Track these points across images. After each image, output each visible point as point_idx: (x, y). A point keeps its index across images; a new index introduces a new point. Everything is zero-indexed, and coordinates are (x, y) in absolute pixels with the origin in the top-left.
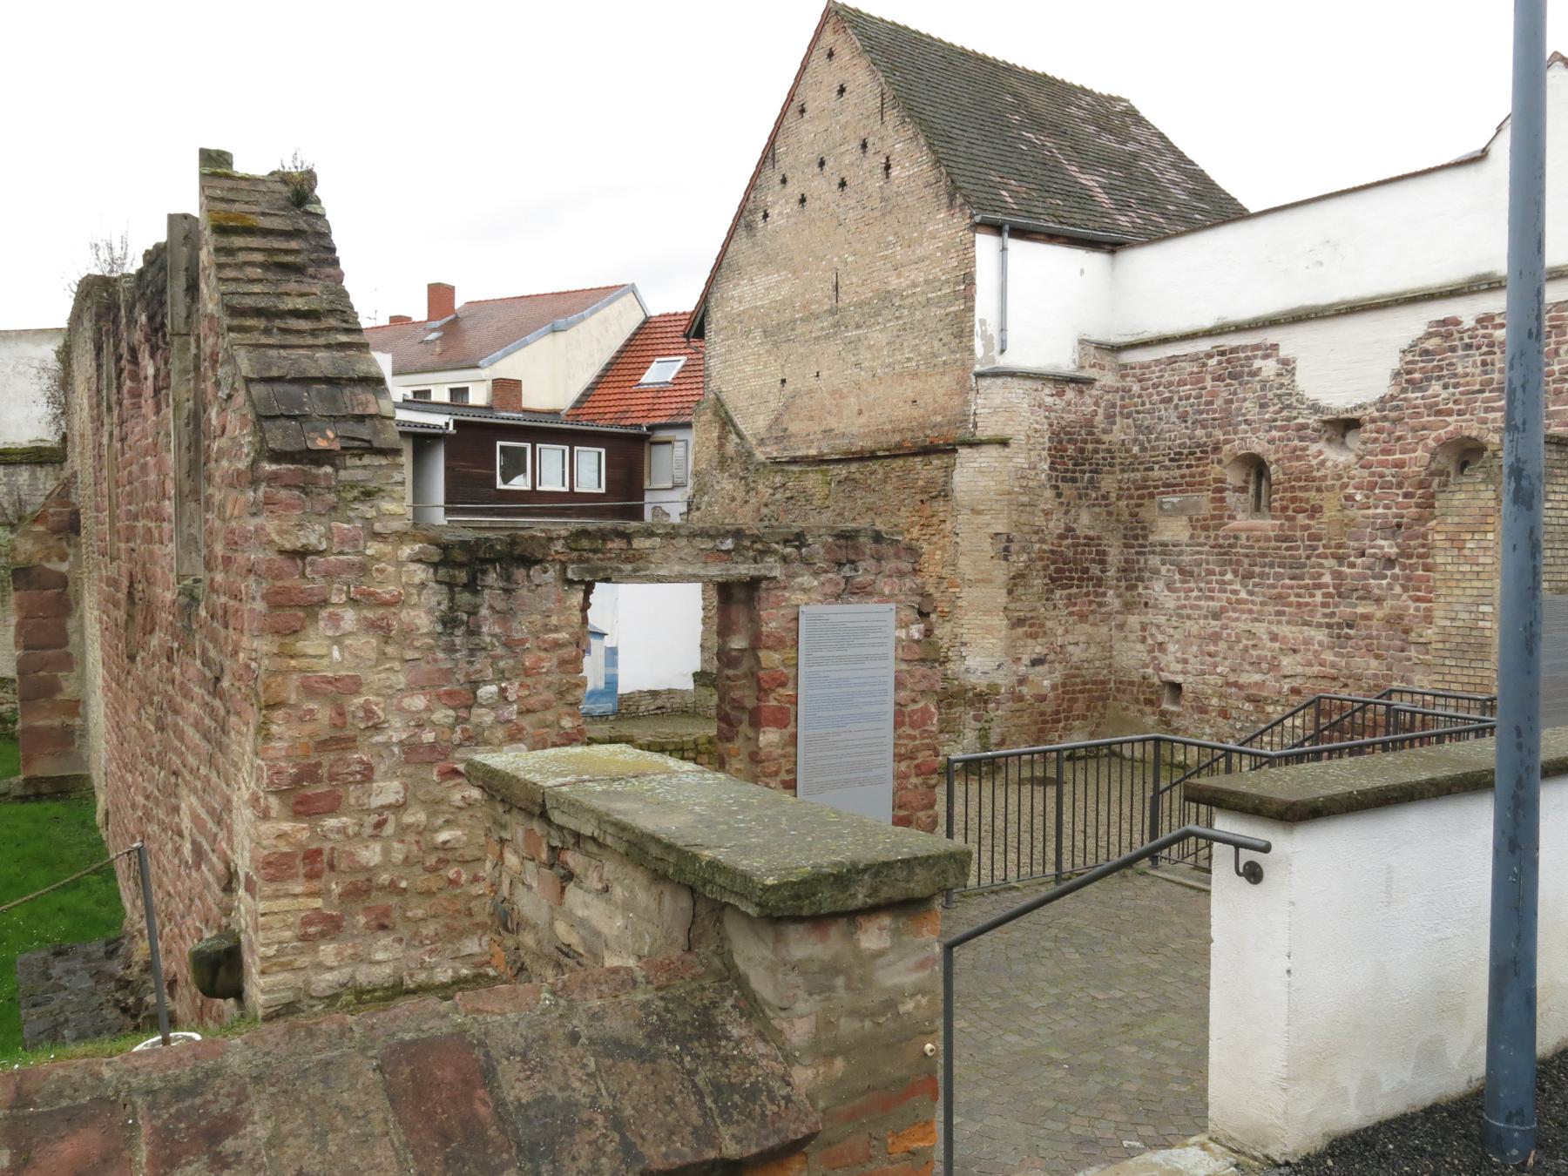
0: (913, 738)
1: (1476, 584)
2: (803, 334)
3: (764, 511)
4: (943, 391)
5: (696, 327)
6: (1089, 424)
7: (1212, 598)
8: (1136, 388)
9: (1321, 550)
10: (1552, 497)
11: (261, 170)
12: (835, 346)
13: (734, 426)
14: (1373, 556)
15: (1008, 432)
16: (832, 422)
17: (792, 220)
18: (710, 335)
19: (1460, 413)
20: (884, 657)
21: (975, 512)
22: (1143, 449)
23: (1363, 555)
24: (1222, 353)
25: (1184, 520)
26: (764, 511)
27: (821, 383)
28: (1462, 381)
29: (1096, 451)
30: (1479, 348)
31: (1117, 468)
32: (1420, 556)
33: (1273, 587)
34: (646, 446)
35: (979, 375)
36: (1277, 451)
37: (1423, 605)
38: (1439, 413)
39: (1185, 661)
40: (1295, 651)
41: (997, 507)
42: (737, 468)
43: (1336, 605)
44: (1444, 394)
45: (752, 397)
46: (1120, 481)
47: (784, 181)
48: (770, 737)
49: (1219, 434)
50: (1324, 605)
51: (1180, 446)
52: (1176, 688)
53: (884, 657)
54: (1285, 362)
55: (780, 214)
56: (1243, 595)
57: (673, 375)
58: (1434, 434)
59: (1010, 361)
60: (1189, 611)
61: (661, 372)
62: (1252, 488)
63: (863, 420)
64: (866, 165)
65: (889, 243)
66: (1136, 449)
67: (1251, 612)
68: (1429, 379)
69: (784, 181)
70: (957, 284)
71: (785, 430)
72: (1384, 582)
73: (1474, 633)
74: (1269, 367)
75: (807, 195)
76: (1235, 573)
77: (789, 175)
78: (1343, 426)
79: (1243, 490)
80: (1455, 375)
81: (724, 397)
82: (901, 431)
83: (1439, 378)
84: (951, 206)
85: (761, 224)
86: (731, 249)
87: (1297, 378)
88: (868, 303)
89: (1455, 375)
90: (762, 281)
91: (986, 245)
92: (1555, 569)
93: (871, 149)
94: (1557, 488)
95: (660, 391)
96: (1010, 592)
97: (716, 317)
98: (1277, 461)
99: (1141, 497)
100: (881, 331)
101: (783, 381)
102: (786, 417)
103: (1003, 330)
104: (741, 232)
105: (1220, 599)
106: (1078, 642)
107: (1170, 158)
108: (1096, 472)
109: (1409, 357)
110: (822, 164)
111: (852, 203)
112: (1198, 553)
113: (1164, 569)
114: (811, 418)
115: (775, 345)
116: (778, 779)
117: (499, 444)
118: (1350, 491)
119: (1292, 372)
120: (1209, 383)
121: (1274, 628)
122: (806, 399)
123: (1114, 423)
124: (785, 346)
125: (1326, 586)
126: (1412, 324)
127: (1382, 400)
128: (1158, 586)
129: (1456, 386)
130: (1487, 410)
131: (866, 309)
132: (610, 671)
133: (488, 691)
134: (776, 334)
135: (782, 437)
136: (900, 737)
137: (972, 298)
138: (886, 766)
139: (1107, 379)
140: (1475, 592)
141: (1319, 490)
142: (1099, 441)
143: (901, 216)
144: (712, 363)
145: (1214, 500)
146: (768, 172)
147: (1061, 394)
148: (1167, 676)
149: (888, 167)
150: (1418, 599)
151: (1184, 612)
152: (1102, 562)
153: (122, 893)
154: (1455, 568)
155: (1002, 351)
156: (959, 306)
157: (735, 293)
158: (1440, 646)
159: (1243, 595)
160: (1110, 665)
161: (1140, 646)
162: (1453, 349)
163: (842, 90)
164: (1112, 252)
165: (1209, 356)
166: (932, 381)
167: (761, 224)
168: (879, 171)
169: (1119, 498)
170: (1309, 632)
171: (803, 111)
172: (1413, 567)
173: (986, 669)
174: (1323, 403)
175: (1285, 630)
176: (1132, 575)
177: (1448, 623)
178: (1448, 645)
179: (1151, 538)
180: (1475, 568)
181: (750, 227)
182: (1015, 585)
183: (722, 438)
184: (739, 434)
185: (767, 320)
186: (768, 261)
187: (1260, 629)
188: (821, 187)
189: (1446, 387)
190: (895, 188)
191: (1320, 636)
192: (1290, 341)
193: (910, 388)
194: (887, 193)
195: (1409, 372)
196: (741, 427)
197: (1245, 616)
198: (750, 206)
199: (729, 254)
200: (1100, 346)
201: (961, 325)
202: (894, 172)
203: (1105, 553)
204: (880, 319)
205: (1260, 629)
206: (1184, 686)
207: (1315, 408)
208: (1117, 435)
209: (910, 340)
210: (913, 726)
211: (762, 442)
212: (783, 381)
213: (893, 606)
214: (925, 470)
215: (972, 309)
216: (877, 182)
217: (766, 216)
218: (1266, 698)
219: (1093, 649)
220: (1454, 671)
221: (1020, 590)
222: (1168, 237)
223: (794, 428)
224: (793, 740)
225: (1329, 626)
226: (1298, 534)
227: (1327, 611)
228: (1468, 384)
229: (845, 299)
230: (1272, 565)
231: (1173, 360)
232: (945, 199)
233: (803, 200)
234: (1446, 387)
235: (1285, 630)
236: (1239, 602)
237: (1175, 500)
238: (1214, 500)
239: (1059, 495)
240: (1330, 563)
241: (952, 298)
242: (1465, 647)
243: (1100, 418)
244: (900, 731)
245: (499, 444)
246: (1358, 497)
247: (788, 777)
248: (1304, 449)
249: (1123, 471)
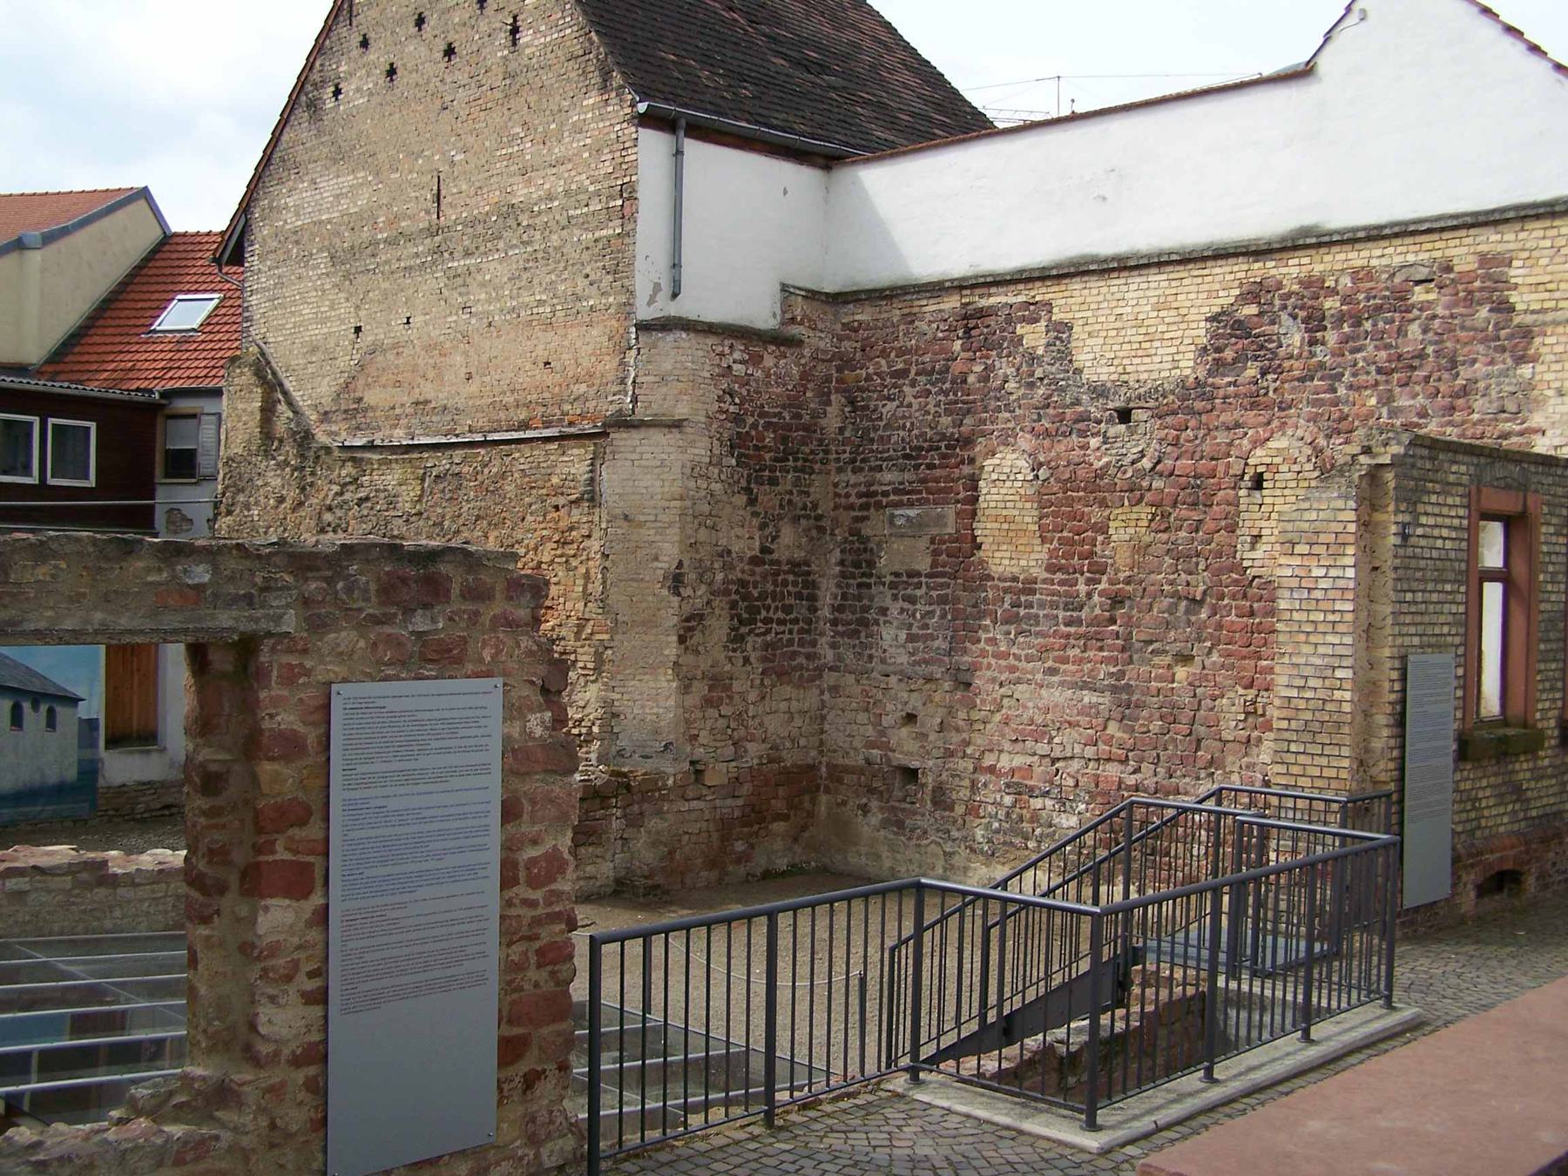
0: (533, 904)
1: (1330, 639)
2: (387, 262)
3: (328, 517)
4: (589, 349)
5: (232, 248)
10: (1423, 520)
12: (435, 280)
13: (285, 393)
16: (428, 391)
17: (376, 100)
18: (252, 261)
20: (484, 769)
26: (328, 517)
27: (412, 333)
31: (833, 465)
34: (160, 420)
42: (290, 450)
45: (314, 350)
46: (836, 485)
47: (365, 44)
48: (278, 918)
52: (911, 774)
53: (484, 769)
55: (358, 90)
57: (199, 321)
59: (686, 307)
61: (184, 314)
63: (474, 387)
64: (483, 26)
65: (514, 137)
69: (365, 44)
70: (611, 197)
71: (360, 399)
73: (1329, 707)
75: (398, 64)
77: (371, 35)
81: (269, 350)
82: (527, 405)
84: (604, 88)
85: (330, 104)
86: (285, 137)
88: (483, 220)
90: (329, 186)
92: (1426, 619)
94: (1429, 509)
95: (184, 339)
96: (682, 640)
97: (262, 232)
100: (501, 260)
101: (358, 330)
102: (361, 382)
104: (302, 115)
106: (778, 719)
107: (901, 55)
108: (802, 470)
110: (420, 22)
111: (462, 78)
114: (398, 384)
115: (347, 276)
116: (292, 989)
117: (93, 426)
122: (390, 356)
123: (829, 403)
124: (361, 279)
126: (1219, 288)
131: (480, 229)
132: (87, 754)
134: (350, 258)
135: (355, 412)
136: (509, 903)
137: (633, 218)
138: (489, 954)
139: (816, 341)
143: (532, 99)
144: (254, 300)
146: (342, 30)
147: (756, 360)
148: (899, 758)
149: (515, 30)
152: (813, 598)
155: (675, 295)
156: (615, 228)
157: (291, 202)
158: (1284, 724)
160: (822, 743)
164: (827, 168)
166: (573, 333)
167: (330, 104)
168: (503, 38)
176: (857, 623)
177: (1294, 693)
178: (1294, 725)
180: (1331, 617)
181: (314, 106)
182: (691, 629)
183: (268, 411)
184: (290, 404)
185: (337, 241)
186: (339, 157)
188: (418, 54)
190: (525, 61)
192: (1069, 301)
193: (544, 343)
194: (513, 66)
195: (1219, 350)
196: (296, 395)
198: (315, 76)
199: (283, 145)
200: (812, 295)
202: (525, 37)
203: (814, 585)
204: (501, 245)
209: (543, 275)
210: (533, 883)
211: (325, 417)
212: (358, 330)
213: (499, 681)
216: (499, 48)
217: (337, 92)
218: (1032, 789)
219: (798, 722)
220: (1301, 759)
221: (697, 637)
222: (905, 153)
223: (372, 397)
224: (322, 917)
229: (450, 215)
232: (596, 79)
233: (392, 72)
237: (912, 513)
239: (752, 502)
241: (603, 217)
242: (1316, 727)
244: (510, 893)
245: (93, 426)
247: (311, 985)
249: (840, 470)
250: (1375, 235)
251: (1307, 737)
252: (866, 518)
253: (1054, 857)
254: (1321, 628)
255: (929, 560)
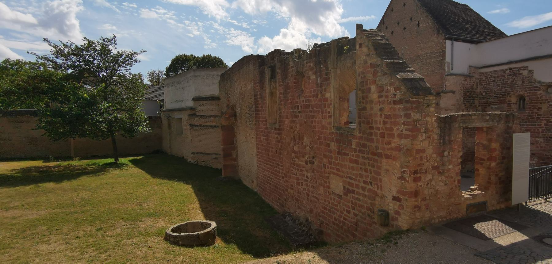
6: (472, 88)
8: (484, 79)
11: (368, 29)
15: (454, 90)
22: (486, 94)
24: (511, 69)
29: (474, 94)
35: (446, 75)
47: (387, 28)
49: (509, 90)
50: (542, 132)
54: (530, 71)
62: (518, 103)
66: (484, 94)
74: (525, 73)
79: (516, 104)
84: (438, 33)
87: (534, 75)
91: (448, 43)
93: (413, 20)
98: (528, 96)
99: (486, 106)
103: (452, 64)
110: (398, 23)
120: (506, 76)
125: (543, 127)
133: (446, 153)
141: (541, 103)
142: (474, 92)
145: (508, 106)
149: (419, 24)
153: (271, 204)
163: (404, 5)
165: (507, 70)
169: (479, 106)
171: (392, 10)
191: (542, 140)
192: (531, 65)
201: (442, 63)
207: (540, 82)
208: (479, 90)
215: (445, 59)
225: (544, 138)
230: (526, 122)
231: (495, 71)
233: (392, 33)
238: (508, 106)
243: (475, 86)
248: (536, 93)
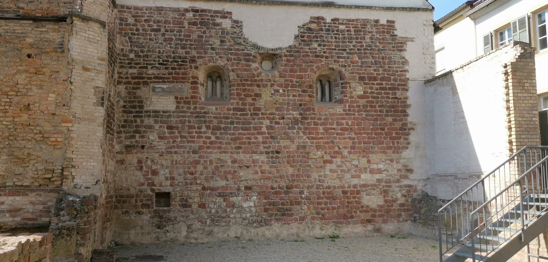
1: (530, 101)
7: (193, 142)
9: (261, 116)
14: (290, 118)
19: (327, 57)
21: (85, 69)
22: (138, 56)
23: (283, 118)
24: (197, 11)
25: (172, 98)
28: (327, 44)
30: (333, 31)
32: (312, 118)
33: (233, 134)
36: (232, 65)
37: (315, 141)
38: (317, 56)
39: (173, 178)
40: (248, 167)
41: (99, 68)
43: (271, 143)
44: (319, 48)
51: (167, 57)
52: (167, 195)
54: (236, 22)
56: (213, 139)
58: (316, 65)
60: (176, 150)
67: (219, 148)
68: (311, 41)
72: (295, 131)
73: (531, 123)
76: (208, 127)
78: (272, 56)
80: (324, 41)
83: (317, 41)
89: (324, 41)
99: (139, 83)
105: (199, 142)
109: (302, 30)
112: (183, 117)
113: (157, 127)
118: (276, 87)
119: (241, 27)
121: (235, 156)
127: (290, 47)
128: (153, 137)
129: (324, 46)
130: (338, 57)
140: (530, 105)
141: (258, 86)
150: (313, 138)
151: (173, 150)
154: (521, 95)
159: (213, 139)
161: (138, 173)
162: (322, 30)
165: (187, 10)
170: (256, 157)
172: (308, 124)
173: (89, 185)
174: (260, 44)
175: (241, 156)
177: (521, 119)
179: (146, 108)
187: (227, 157)
189: (319, 45)
197: (215, 151)
205: (227, 157)
206: (173, 194)
214: (51, 33)
220: (525, 140)
225: (267, 153)
226: (247, 107)
227: (266, 145)
228: (330, 46)
230: (232, 123)
234: (319, 45)
235: (241, 156)
236: (211, 143)
240: (267, 122)
242: (529, 129)
246: (281, 91)
250: (358, 7)
251: (526, 133)
252: (139, 88)
253: (491, 176)
254: (527, 98)
255: (175, 106)
